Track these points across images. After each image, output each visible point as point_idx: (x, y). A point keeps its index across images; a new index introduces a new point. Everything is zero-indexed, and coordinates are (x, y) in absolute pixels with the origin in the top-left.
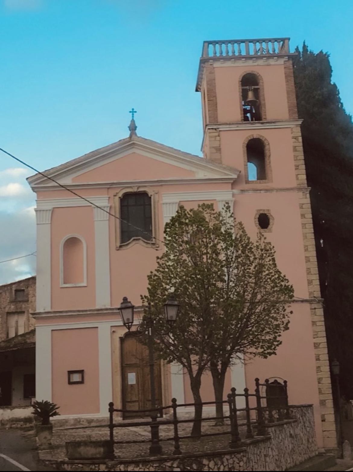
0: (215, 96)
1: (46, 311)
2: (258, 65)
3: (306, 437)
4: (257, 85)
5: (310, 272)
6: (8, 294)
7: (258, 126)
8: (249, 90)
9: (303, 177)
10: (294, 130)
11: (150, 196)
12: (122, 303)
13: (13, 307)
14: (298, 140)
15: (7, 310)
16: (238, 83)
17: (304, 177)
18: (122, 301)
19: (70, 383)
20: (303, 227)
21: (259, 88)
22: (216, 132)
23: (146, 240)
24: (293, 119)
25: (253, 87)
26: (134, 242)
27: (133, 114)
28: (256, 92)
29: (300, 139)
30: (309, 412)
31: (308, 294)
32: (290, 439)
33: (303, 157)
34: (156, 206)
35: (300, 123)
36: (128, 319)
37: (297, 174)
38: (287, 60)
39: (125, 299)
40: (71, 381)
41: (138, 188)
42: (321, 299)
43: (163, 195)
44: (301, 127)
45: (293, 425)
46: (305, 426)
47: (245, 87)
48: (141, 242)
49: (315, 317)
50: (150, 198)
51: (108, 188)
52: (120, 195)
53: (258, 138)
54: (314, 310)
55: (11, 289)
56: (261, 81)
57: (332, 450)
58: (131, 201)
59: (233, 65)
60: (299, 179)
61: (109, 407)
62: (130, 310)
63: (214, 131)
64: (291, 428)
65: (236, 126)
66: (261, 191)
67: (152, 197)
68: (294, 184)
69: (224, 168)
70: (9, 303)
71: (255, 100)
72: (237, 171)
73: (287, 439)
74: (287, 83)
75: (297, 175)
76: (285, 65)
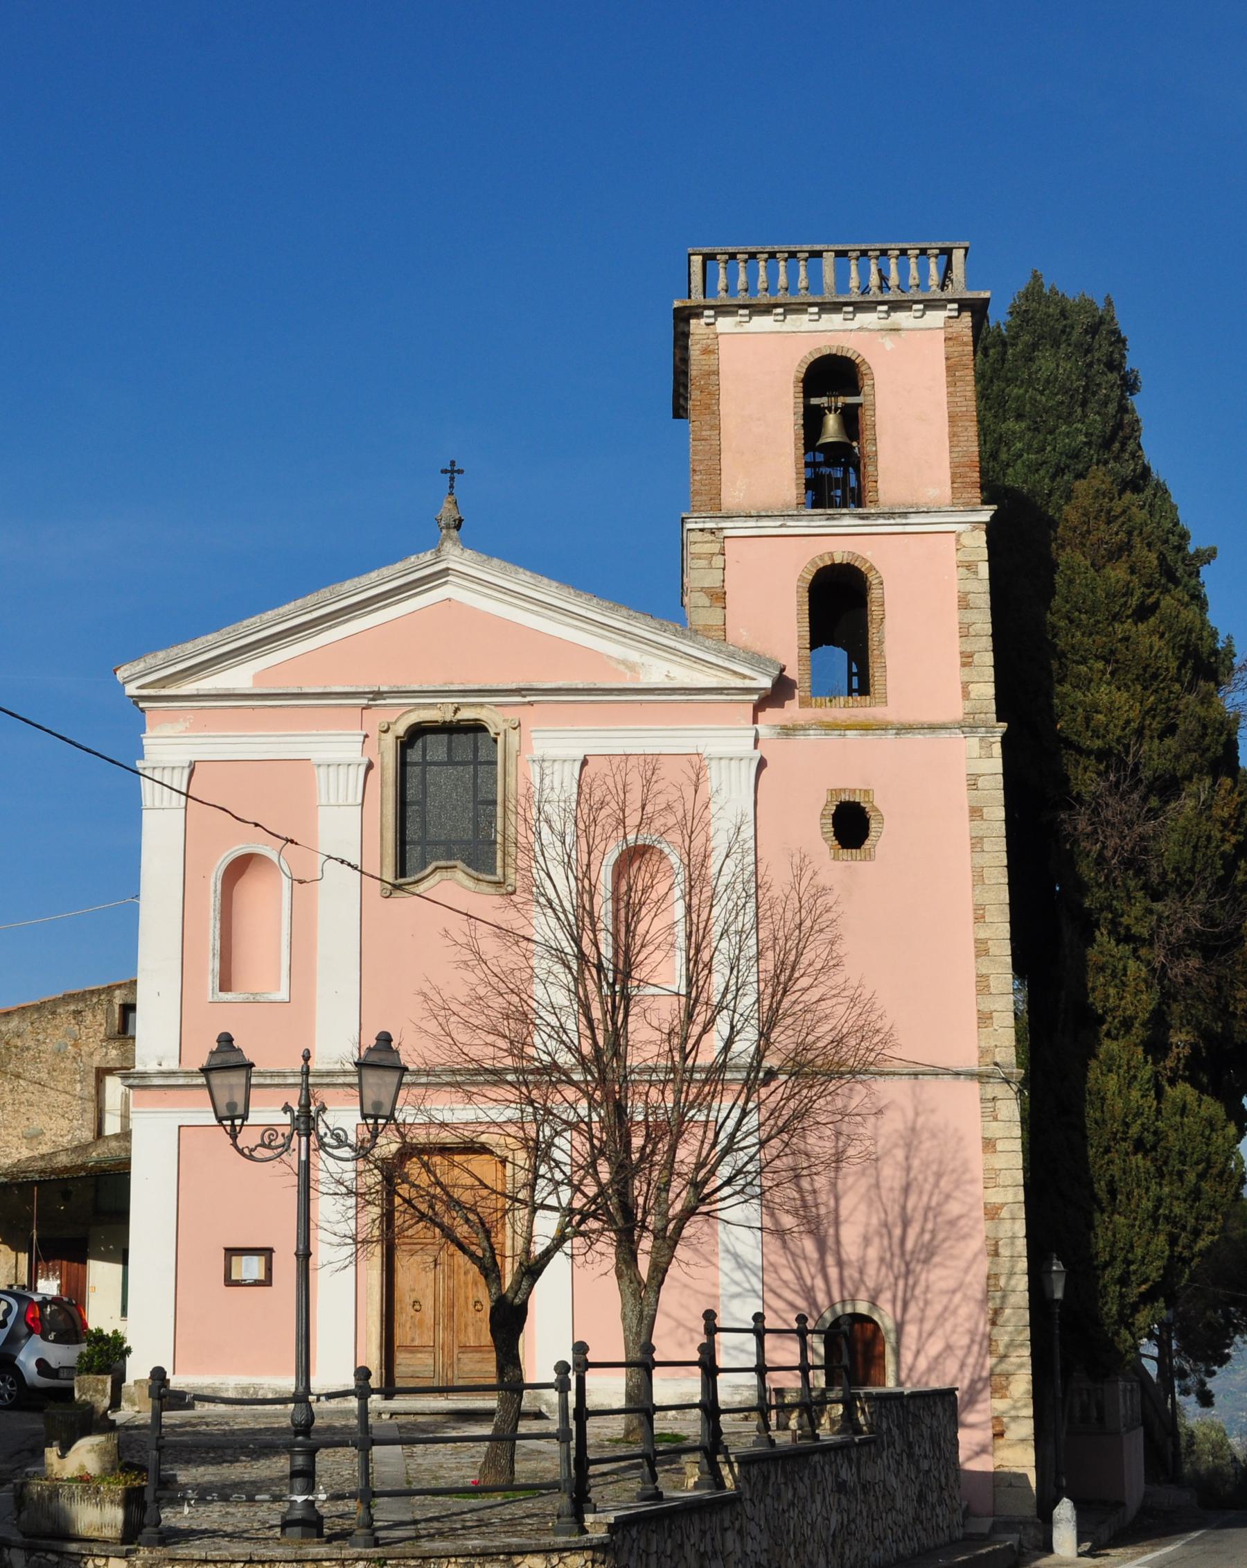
0: (718, 428)
1: (164, 1068)
2: (860, 329)
3: (913, 1491)
4: (858, 394)
5: (988, 986)
6: (100, 1017)
7: (847, 522)
8: (829, 409)
9: (986, 690)
10: (965, 540)
11: (492, 735)
12: (212, 1053)
13: (114, 1052)
14: (976, 573)
15: (97, 1061)
16: (791, 386)
17: (990, 690)
18: (215, 1046)
19: (229, 1282)
20: (973, 846)
21: (861, 405)
22: (712, 542)
23: (476, 870)
24: (964, 504)
25: (841, 401)
26: (438, 876)
27: (452, 479)
28: (851, 419)
29: (984, 570)
30: (939, 1410)
31: (976, 1054)
32: (831, 1499)
33: (988, 628)
34: (511, 769)
35: (987, 519)
36: (232, 1106)
37: (966, 679)
38: (955, 314)
39: (226, 1040)
40: (234, 1277)
41: (456, 710)
42: (1015, 1070)
43: (534, 735)
44: (988, 533)
45: (788, 1468)
46: (910, 1456)
47: (814, 401)
48: (459, 875)
49: (995, 1123)
50: (495, 741)
51: (367, 707)
52: (401, 729)
53: (848, 564)
54: (990, 1105)
55: (110, 1001)
56: (868, 382)
57: (1020, 1523)
58: (437, 747)
59: (778, 327)
60: (972, 696)
61: (704, 1322)
62: (391, 1078)
63: (711, 538)
64: (846, 1465)
65: (779, 523)
66: (848, 732)
67: (500, 739)
68: (956, 710)
69: (731, 656)
70: (102, 1041)
71: (847, 441)
72: (772, 662)
73: (818, 1498)
74: (951, 389)
75: (965, 686)
76: (950, 330)
